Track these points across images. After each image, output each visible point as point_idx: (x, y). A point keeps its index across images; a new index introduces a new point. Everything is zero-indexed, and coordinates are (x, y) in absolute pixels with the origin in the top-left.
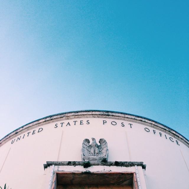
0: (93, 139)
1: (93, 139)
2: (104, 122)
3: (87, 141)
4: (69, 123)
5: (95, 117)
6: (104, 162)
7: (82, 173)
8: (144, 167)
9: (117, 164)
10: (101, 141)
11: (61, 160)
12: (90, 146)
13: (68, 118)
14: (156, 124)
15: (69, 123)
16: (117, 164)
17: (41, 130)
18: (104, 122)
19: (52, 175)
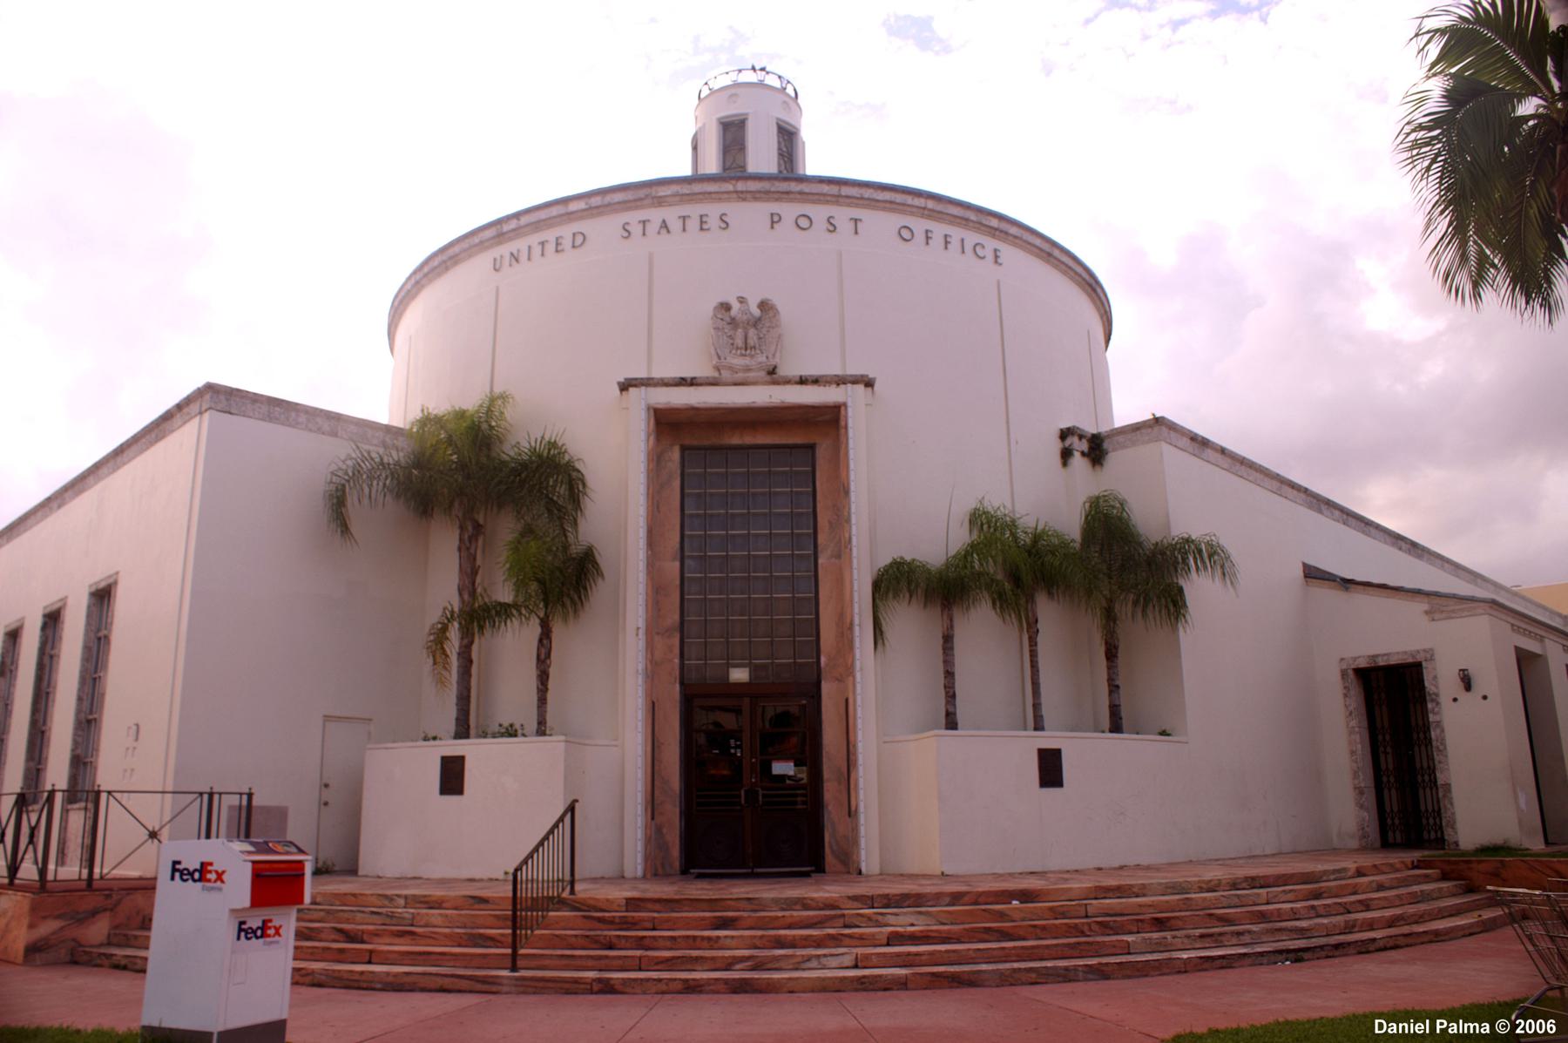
0: (742, 300)
1: (742, 300)
2: (775, 220)
3: (726, 307)
4: (664, 225)
5: (744, 200)
6: (772, 375)
7: (594, 980)
8: (869, 384)
9: (802, 381)
10: (764, 305)
11: (657, 373)
12: (733, 322)
13: (660, 202)
14: (939, 207)
15: (664, 225)
16: (802, 381)
17: (579, 239)
18: (775, 220)
19: (643, 415)
